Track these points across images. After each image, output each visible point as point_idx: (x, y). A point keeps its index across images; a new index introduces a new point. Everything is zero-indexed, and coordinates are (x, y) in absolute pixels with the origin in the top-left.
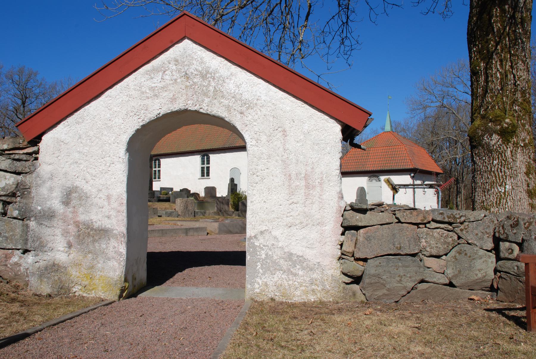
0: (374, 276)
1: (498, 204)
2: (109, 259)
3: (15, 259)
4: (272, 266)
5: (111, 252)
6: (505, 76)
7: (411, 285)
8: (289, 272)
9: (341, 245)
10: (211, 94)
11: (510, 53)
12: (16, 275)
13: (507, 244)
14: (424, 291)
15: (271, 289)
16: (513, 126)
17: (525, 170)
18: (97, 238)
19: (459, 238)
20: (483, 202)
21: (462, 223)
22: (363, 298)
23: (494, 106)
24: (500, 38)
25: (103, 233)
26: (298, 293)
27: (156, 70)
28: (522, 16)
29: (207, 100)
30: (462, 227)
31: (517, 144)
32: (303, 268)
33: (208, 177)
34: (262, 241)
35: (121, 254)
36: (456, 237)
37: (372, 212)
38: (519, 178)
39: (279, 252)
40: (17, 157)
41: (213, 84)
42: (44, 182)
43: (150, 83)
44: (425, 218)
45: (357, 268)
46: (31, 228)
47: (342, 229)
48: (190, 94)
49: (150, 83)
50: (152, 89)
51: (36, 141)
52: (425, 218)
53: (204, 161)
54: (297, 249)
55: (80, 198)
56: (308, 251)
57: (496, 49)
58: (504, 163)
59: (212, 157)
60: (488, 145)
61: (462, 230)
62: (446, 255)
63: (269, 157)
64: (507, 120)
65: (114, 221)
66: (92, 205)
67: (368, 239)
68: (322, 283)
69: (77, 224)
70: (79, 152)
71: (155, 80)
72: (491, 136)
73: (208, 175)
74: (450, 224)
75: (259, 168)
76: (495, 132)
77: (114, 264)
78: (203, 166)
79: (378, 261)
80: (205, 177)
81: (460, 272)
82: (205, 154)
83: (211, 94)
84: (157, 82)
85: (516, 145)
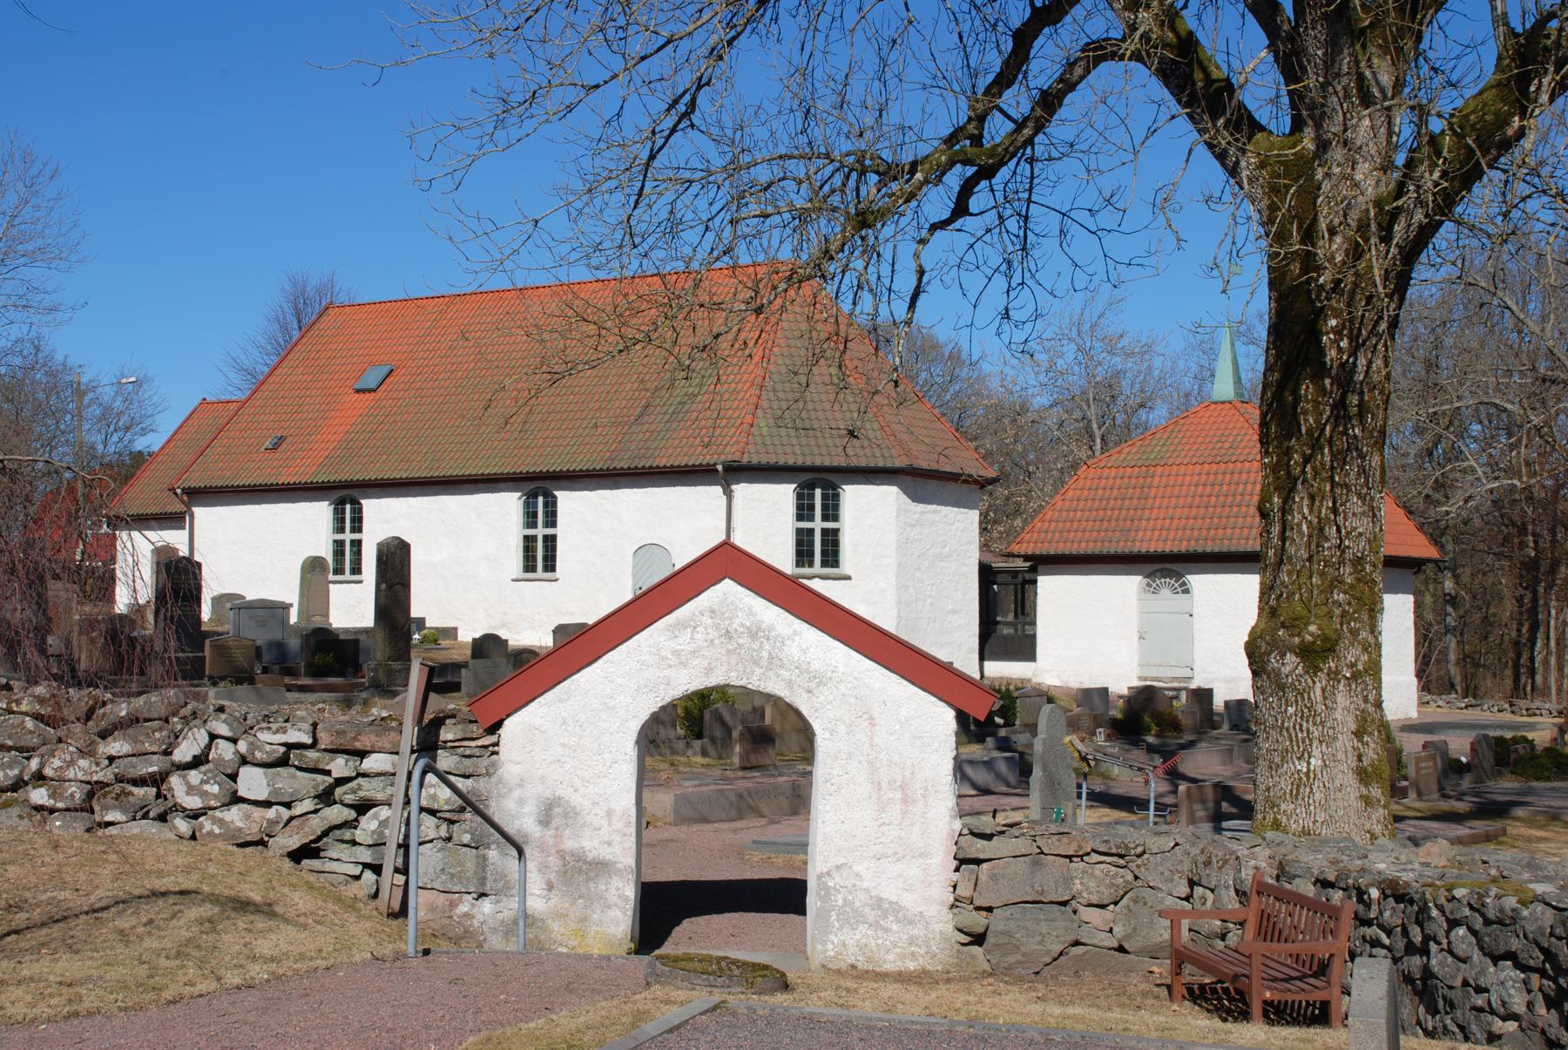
0: (1002, 933)
1: (1295, 796)
2: (609, 907)
3: (463, 908)
4: (852, 917)
5: (612, 897)
6: (1319, 530)
7: (1058, 948)
8: (876, 926)
9: (955, 887)
10: (764, 662)
11: (1332, 479)
12: (466, 932)
13: (1201, 889)
14: (1079, 958)
15: (851, 951)
16: (1325, 638)
17: (1353, 727)
18: (592, 875)
19: (1136, 878)
20: (1268, 789)
21: (1139, 856)
22: (987, 967)
23: (1291, 595)
24: (1313, 447)
25: (601, 867)
26: (890, 957)
27: (681, 625)
28: (1361, 401)
29: (758, 671)
30: (1139, 861)
31: (1337, 672)
32: (898, 921)
33: (549, 575)
34: (838, 879)
35: (626, 899)
36: (1130, 877)
37: (1001, 838)
38: (1339, 744)
39: (862, 897)
40: (468, 752)
41: (767, 647)
42: (510, 790)
43: (673, 645)
44: (1080, 847)
45: (978, 921)
46: (491, 861)
47: (955, 863)
48: (733, 662)
49: (673, 645)
50: (677, 653)
51: (494, 728)
52: (1080, 847)
53: (535, 515)
54: (890, 893)
55: (566, 815)
56: (905, 894)
57: (1303, 472)
58: (1309, 713)
59: (567, 500)
60: (1278, 673)
61: (1138, 866)
62: (1116, 903)
63: (850, 756)
64: (1312, 628)
65: (617, 849)
66: (584, 825)
67: (994, 878)
68: (926, 942)
69: (562, 854)
70: (563, 745)
71: (681, 640)
72: (1283, 655)
73: (550, 565)
74: (1122, 856)
75: (835, 772)
76: (1291, 649)
77: (616, 913)
78: (531, 532)
79: (1009, 911)
80: (347, 576)
81: (1135, 930)
82: (539, 488)
83: (764, 662)
84: (684, 642)
85: (1334, 675)
